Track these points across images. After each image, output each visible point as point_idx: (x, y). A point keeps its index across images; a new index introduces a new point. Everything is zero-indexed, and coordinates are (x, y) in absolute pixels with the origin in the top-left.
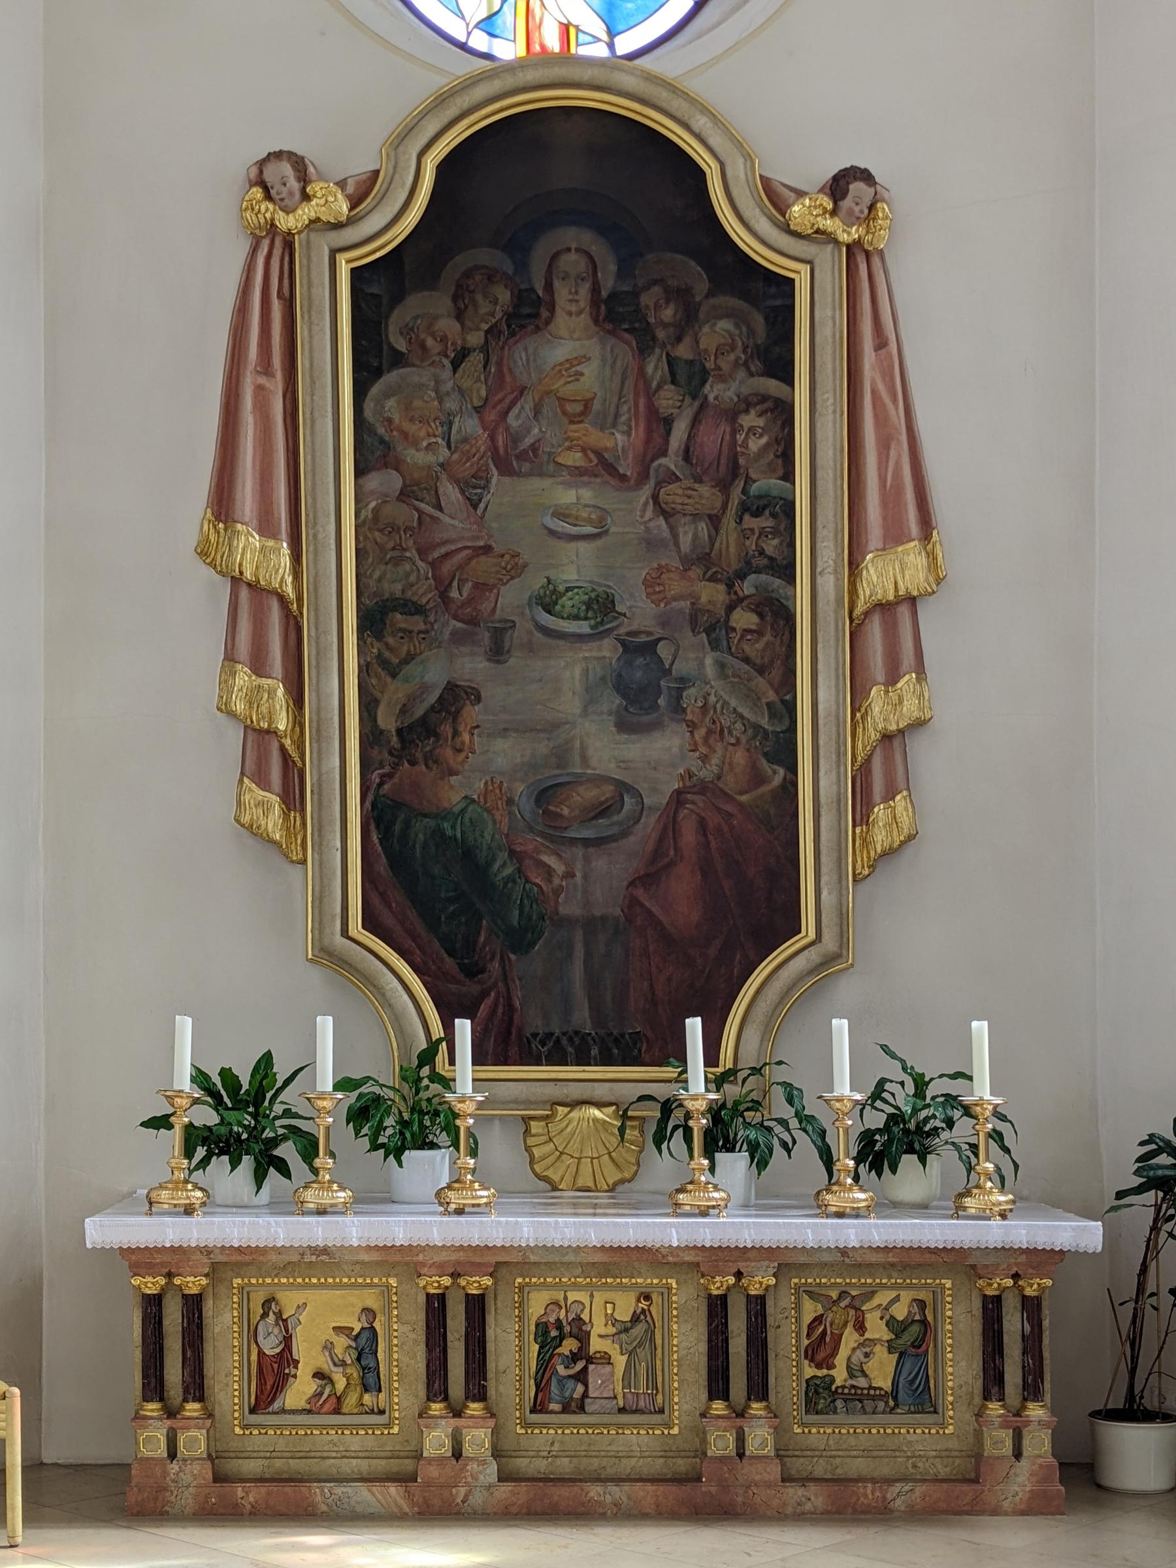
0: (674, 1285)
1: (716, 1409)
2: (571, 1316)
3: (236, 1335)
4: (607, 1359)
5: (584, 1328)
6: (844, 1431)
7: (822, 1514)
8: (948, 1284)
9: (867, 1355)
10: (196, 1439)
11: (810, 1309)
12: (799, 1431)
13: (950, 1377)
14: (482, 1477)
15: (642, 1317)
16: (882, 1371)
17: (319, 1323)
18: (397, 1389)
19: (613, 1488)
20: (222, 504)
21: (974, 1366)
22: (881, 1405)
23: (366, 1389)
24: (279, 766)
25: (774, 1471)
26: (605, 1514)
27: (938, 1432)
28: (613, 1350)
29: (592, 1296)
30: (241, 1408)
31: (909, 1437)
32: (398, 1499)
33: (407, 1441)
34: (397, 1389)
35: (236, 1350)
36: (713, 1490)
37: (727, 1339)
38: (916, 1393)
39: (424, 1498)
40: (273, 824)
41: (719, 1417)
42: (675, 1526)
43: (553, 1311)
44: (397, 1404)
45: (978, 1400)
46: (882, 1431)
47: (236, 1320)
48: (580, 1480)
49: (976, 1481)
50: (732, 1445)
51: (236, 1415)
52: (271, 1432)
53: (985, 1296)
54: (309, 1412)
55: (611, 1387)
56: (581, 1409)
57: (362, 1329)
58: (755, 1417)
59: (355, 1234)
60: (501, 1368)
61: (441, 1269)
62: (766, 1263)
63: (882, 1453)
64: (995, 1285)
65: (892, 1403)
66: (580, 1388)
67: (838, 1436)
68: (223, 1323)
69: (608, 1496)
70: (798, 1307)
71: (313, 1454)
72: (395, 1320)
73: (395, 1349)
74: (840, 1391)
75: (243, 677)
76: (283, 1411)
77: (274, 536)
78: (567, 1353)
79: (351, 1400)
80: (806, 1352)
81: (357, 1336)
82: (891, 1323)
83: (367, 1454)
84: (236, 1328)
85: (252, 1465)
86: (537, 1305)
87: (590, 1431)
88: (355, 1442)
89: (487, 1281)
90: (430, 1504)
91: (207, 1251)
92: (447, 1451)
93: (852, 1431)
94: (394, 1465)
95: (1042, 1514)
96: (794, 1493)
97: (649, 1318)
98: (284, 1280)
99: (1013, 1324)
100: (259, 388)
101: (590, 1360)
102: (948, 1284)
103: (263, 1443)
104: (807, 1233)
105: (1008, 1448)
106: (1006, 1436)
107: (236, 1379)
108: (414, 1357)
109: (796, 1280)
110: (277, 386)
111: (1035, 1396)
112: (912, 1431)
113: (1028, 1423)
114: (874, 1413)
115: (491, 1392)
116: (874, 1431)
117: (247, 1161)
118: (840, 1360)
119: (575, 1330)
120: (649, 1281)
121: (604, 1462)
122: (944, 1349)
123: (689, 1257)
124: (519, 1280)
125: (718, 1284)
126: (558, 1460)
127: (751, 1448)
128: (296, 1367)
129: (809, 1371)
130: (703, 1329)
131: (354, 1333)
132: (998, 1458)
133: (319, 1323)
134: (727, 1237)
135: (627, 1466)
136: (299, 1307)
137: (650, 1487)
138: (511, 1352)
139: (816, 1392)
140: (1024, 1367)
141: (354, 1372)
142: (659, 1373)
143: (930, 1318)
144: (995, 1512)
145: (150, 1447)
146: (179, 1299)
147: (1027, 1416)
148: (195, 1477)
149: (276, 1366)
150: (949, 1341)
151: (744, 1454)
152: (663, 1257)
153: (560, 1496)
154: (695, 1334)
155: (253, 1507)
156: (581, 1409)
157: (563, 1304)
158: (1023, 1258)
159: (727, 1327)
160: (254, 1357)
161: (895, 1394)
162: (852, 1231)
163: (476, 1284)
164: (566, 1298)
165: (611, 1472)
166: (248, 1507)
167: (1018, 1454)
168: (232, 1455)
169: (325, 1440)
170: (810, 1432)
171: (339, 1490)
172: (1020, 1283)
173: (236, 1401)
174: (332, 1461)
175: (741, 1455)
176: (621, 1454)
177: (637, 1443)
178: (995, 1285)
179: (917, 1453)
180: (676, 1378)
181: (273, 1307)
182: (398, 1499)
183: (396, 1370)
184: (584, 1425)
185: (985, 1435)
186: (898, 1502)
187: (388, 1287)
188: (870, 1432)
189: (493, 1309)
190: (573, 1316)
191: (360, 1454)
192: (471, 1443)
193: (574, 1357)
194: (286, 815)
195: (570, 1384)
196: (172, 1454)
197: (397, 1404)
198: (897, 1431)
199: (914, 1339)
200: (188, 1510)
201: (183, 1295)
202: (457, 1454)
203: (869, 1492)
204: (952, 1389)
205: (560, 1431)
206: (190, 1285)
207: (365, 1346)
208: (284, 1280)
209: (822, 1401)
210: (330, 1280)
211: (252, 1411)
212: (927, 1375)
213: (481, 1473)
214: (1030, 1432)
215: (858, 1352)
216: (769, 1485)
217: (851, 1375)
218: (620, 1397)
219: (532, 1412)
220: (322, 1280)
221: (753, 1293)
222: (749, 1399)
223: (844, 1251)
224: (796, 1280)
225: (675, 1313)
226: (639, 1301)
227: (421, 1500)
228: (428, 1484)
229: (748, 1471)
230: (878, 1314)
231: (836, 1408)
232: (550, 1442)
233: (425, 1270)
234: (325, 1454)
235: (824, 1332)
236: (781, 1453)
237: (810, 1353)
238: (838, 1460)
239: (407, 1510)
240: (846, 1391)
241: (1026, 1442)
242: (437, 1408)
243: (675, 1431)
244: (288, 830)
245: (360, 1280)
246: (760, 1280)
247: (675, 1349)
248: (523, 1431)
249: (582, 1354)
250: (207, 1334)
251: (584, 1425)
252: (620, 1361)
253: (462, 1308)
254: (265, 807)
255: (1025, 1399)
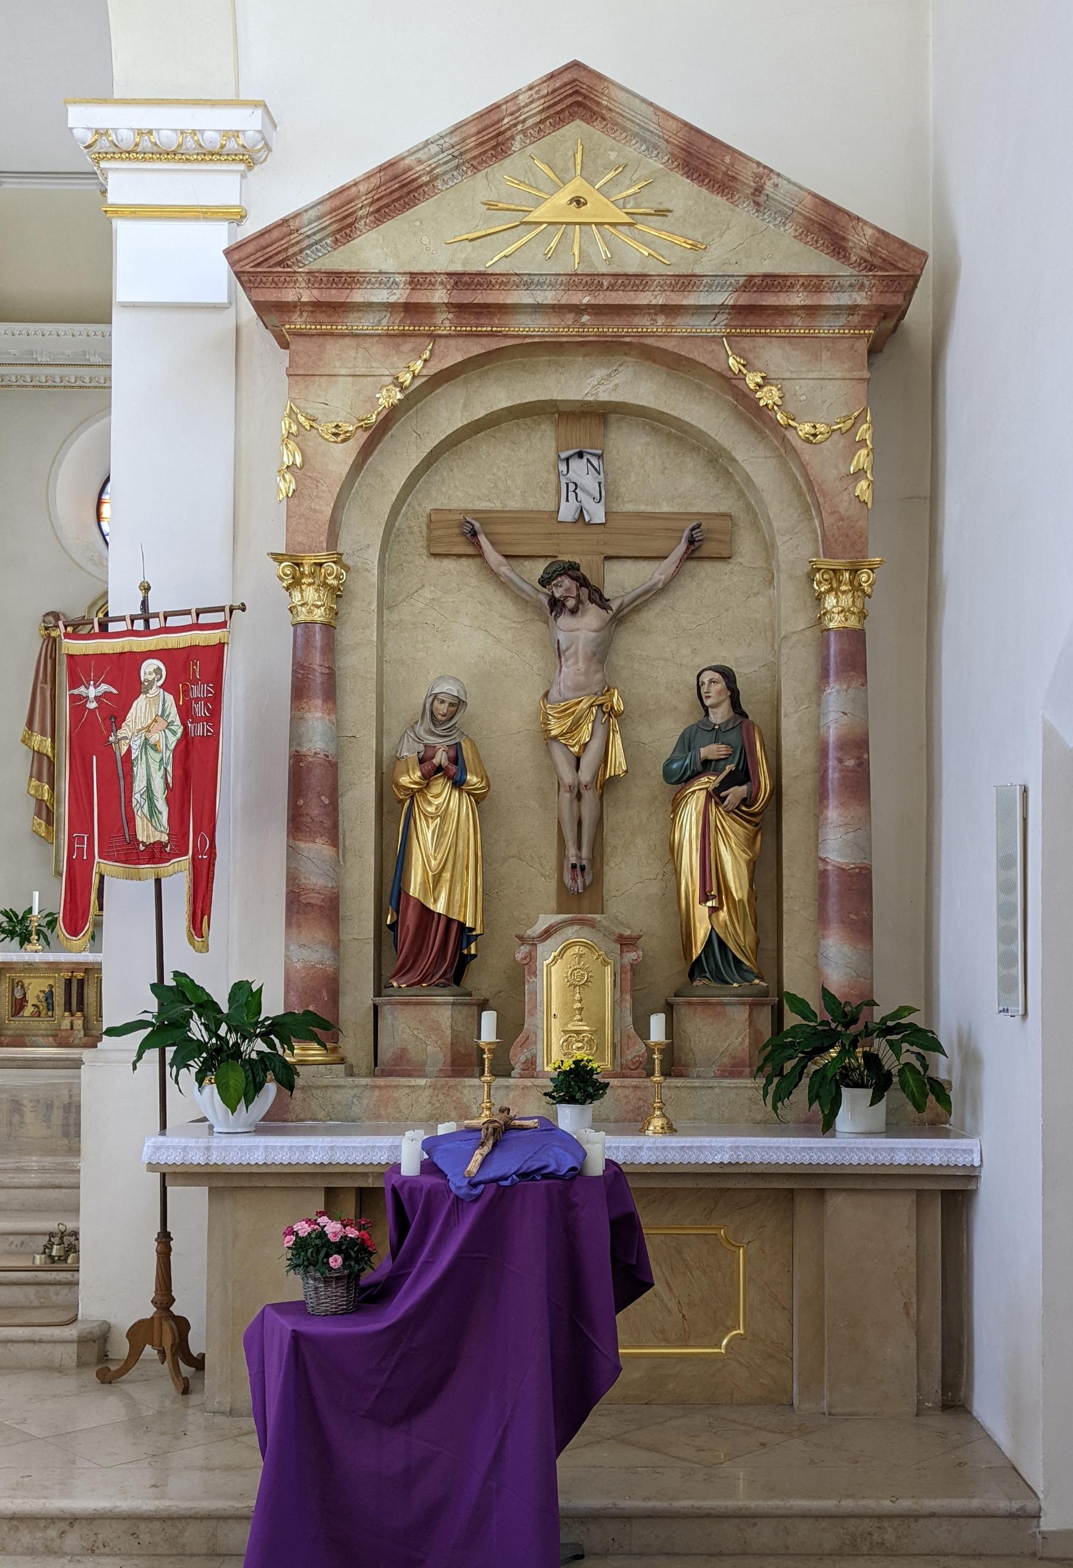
17: (35, 989)
20: (30, 724)
24: (46, 812)
40: (42, 831)
61: (67, 970)
75: (34, 782)
77: (45, 736)
79: (43, 1013)
88: (43, 1026)
92: (69, 1027)
100: (42, 688)
110: (48, 687)
117: (17, 939)
141: (45, 1004)
163: (80, 975)
194: (47, 828)
202: (72, 1028)
207: (49, 996)
244: (48, 832)
254: (40, 824)
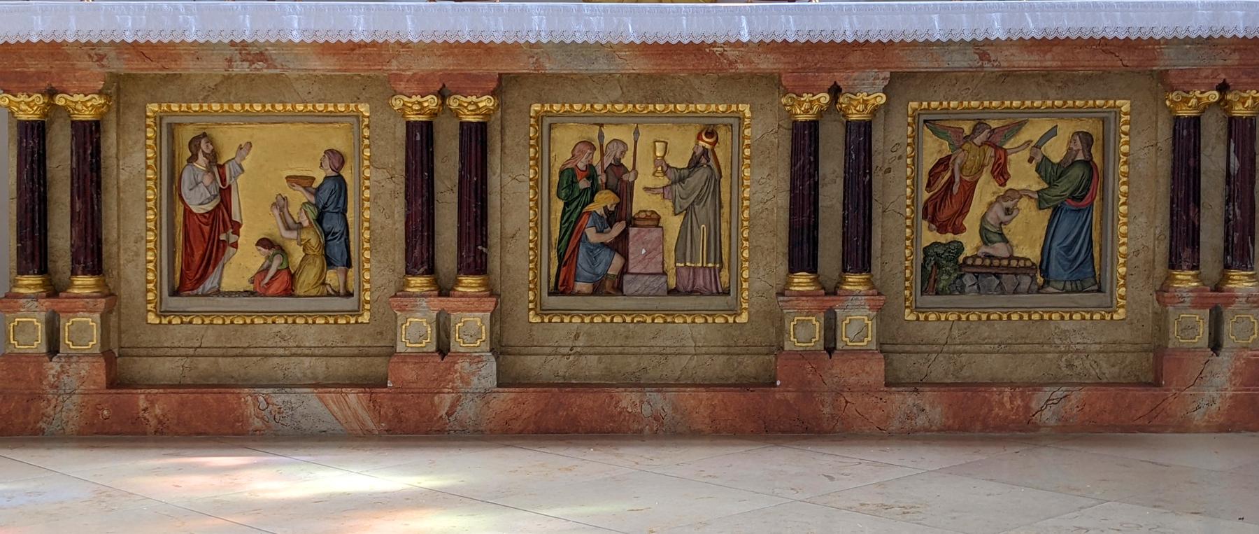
0: (748, 114)
1: (799, 284)
2: (608, 161)
3: (150, 184)
4: (654, 220)
5: (625, 177)
6: (973, 317)
7: (939, 431)
8: (1125, 106)
9: (1008, 211)
10: (86, 328)
11: (933, 149)
12: (912, 317)
13: (1123, 240)
14: (475, 380)
15: (703, 160)
16: (1027, 236)
17: (269, 169)
18: (368, 261)
19: (654, 396)
21: (1158, 222)
22: (1026, 281)
23: (330, 263)
25: (875, 370)
26: (641, 431)
27: (1103, 318)
28: (663, 208)
29: (637, 133)
30: (158, 286)
31: (1063, 326)
32: (360, 411)
33: (381, 333)
34: (368, 261)
35: (151, 204)
36: (790, 396)
37: (816, 184)
38: (1074, 264)
39: (396, 409)
41: (801, 294)
42: (734, 445)
43: (583, 152)
44: (368, 281)
45: (1160, 270)
46: (1026, 317)
47: (150, 162)
48: (611, 386)
49: (1157, 383)
50: (818, 334)
51: (151, 296)
52: (197, 321)
53: (1177, 119)
54: (252, 294)
55: (659, 258)
56: (619, 289)
57: (326, 178)
58: (851, 293)
59: (296, 25)
60: (509, 230)
61: (422, 84)
62: (873, 73)
63: (1025, 348)
64: (1193, 101)
65: (1040, 280)
66: (617, 261)
67: (964, 325)
68: (133, 165)
69: (645, 406)
70: (917, 143)
71: (252, 351)
72: (366, 163)
73: (367, 204)
74: (969, 262)
76: (218, 293)
78: (600, 211)
79: (308, 278)
80: (925, 209)
81: (318, 189)
82: (1044, 168)
83: (325, 351)
84: (150, 174)
85: (168, 365)
86: (564, 146)
87: (628, 319)
88: (311, 334)
89: (486, 102)
90: (403, 415)
91: (94, 50)
92: (429, 344)
93: (984, 317)
94: (361, 366)
95: (1247, 430)
96: (902, 401)
97: (712, 163)
98: (216, 107)
99: (1215, 159)
101: (631, 222)
102: (1125, 106)
103: (182, 336)
104: (932, 21)
105: (1202, 336)
106: (1200, 320)
107: (151, 245)
108: (391, 216)
109: (914, 105)
111: (1242, 261)
112: (1067, 316)
113: (1231, 299)
114: (1015, 292)
115: (494, 264)
116: (1015, 317)
118: (972, 221)
119: (613, 181)
120: (713, 107)
121: (645, 362)
122: (1115, 199)
123: (766, 64)
124: (536, 107)
125: (806, 106)
126: (583, 358)
127: (846, 338)
128: (237, 233)
129: (929, 236)
130: (784, 174)
131: (315, 185)
132: (1188, 350)
133: (269, 169)
134: (820, 28)
135: (676, 367)
136: (241, 148)
137: (703, 394)
138: (522, 208)
139: (938, 265)
140: (1227, 221)
141: (312, 237)
142: (725, 241)
143: (1097, 159)
144: (1183, 427)
145: (21, 338)
146: (68, 131)
147: (1231, 290)
148: (82, 380)
149: (207, 228)
150: (1124, 188)
151: (835, 348)
152: (731, 63)
153: (580, 406)
154: (773, 182)
155: (160, 422)
156: (619, 289)
157: (597, 144)
158: (1234, 59)
159: (817, 169)
160: (180, 218)
161: (1044, 267)
162: (996, 16)
163: (474, 106)
164: (601, 136)
165: (653, 374)
166: (153, 422)
167: (1216, 345)
168: (143, 352)
169: (268, 331)
170: (926, 319)
171: (279, 399)
172: (1229, 97)
173: (151, 276)
174: (276, 360)
175: (830, 349)
176: (668, 350)
177: (691, 334)
178: (1193, 101)
179: (1074, 347)
180: (746, 244)
181: (203, 145)
182: (360, 411)
183: (367, 235)
184: (623, 312)
185: (1172, 318)
186: (1047, 414)
187: (358, 117)
188: (1009, 318)
189: (498, 146)
190: (611, 160)
191: (317, 351)
192: (463, 333)
193: (611, 218)
195: (604, 255)
196: (53, 348)
197: (368, 281)
198: (1046, 317)
199: (1075, 190)
200: (70, 428)
201: (73, 122)
202: (443, 349)
203: (1006, 399)
204: (1125, 256)
205: (587, 320)
206: (79, 107)
207: (330, 203)
208: (216, 107)
209: (945, 277)
210: (279, 107)
211: (175, 293)
212: (1091, 241)
213: (473, 374)
214: (1234, 313)
215: (997, 208)
216: (868, 390)
217: (986, 241)
218: (671, 273)
219: (550, 294)
220: (268, 107)
221: (854, 117)
222: (845, 271)
223: (983, 48)
224: (914, 105)
225: (747, 152)
226: (699, 137)
227: (391, 413)
228: (401, 390)
229: (839, 370)
230: (1026, 154)
231: (963, 286)
232: (573, 335)
233: (401, 86)
234: (270, 351)
235: (951, 181)
236: (887, 347)
237: (930, 210)
238: (964, 358)
239: (371, 425)
240: (979, 262)
241: (1228, 327)
242: (418, 283)
243: (744, 318)
245: (320, 107)
246: (864, 99)
247: (746, 203)
248: (538, 320)
249: (620, 214)
250: (109, 182)
251: (623, 312)
252: (673, 224)
253: (455, 145)
255: (1227, 267)
